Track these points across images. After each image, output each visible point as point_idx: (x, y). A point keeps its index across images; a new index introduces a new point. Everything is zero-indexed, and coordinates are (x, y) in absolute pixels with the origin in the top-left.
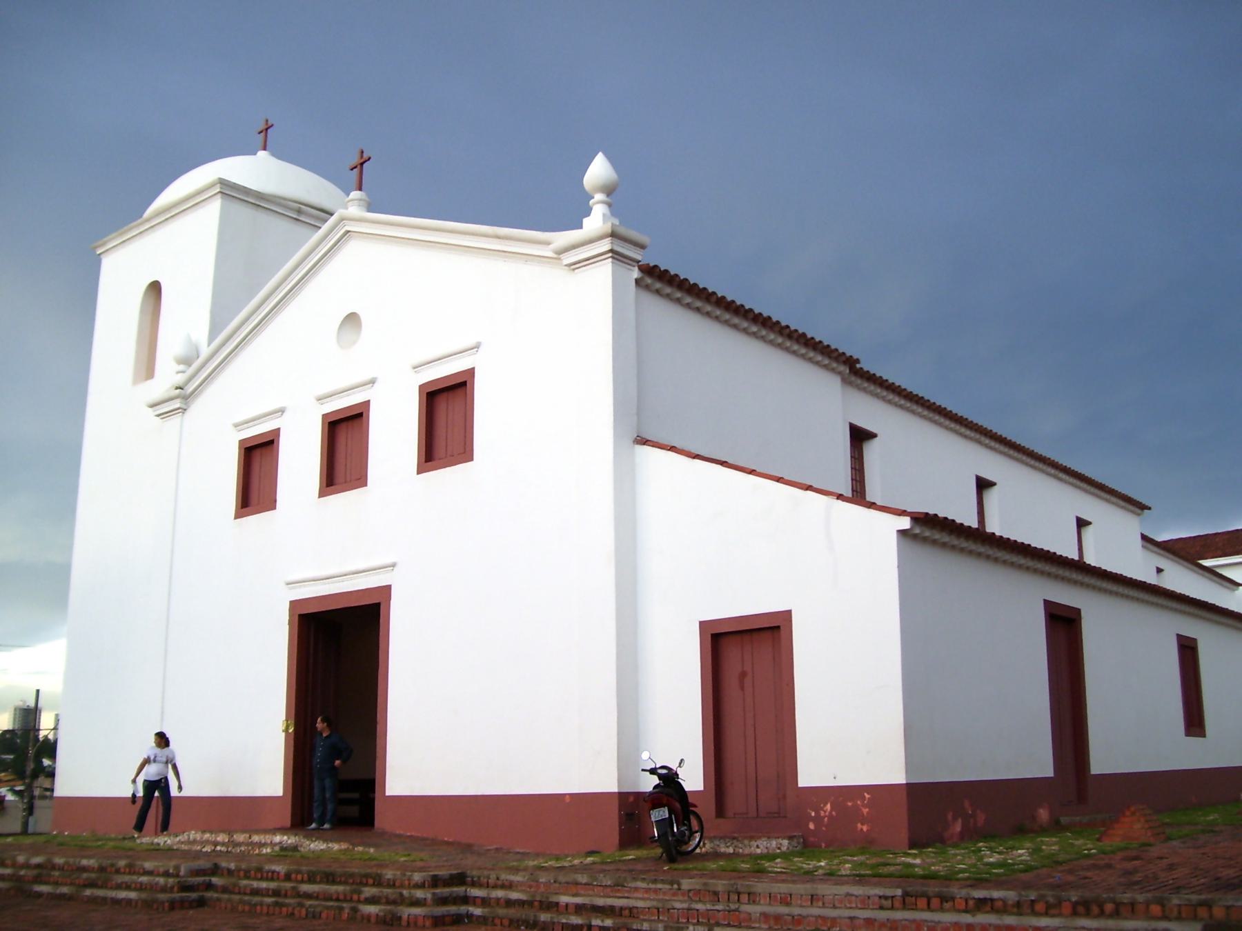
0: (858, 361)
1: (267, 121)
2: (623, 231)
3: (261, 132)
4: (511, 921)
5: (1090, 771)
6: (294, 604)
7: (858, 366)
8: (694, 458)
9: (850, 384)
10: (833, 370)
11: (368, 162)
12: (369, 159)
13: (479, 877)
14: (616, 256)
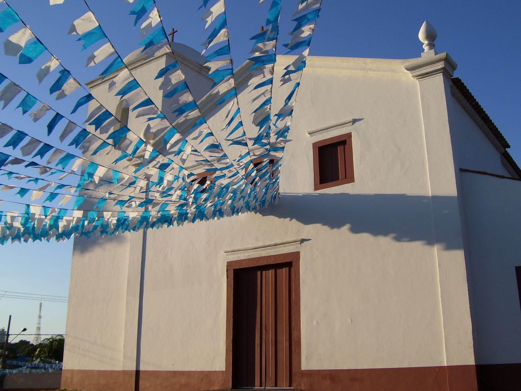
1: (173, 29)
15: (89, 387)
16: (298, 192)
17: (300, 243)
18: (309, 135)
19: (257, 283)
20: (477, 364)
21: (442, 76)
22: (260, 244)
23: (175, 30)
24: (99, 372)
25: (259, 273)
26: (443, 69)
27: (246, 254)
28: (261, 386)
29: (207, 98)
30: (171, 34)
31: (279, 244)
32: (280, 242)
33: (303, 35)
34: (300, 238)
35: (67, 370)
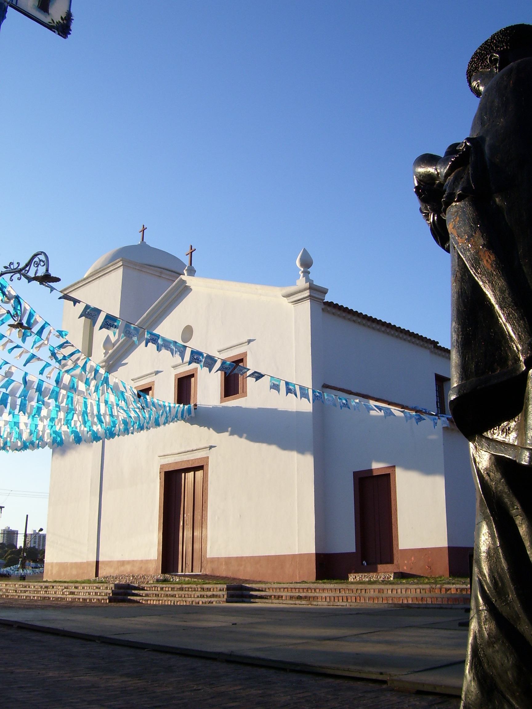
0: (438, 343)
1: (144, 226)
2: (312, 294)
4: (156, 594)
5: (398, 545)
7: (438, 345)
8: (350, 394)
10: (425, 347)
11: (194, 252)
12: (195, 250)
13: (142, 594)
14: (312, 298)
17: (209, 449)
18: (218, 353)
20: (320, 552)
21: (310, 302)
23: (145, 227)
24: (72, 564)
25: (183, 474)
26: (310, 296)
27: (173, 459)
28: (182, 572)
29: (147, 315)
30: (141, 231)
31: (195, 450)
32: (195, 449)
33: (482, 90)
34: (208, 445)
35: (48, 563)
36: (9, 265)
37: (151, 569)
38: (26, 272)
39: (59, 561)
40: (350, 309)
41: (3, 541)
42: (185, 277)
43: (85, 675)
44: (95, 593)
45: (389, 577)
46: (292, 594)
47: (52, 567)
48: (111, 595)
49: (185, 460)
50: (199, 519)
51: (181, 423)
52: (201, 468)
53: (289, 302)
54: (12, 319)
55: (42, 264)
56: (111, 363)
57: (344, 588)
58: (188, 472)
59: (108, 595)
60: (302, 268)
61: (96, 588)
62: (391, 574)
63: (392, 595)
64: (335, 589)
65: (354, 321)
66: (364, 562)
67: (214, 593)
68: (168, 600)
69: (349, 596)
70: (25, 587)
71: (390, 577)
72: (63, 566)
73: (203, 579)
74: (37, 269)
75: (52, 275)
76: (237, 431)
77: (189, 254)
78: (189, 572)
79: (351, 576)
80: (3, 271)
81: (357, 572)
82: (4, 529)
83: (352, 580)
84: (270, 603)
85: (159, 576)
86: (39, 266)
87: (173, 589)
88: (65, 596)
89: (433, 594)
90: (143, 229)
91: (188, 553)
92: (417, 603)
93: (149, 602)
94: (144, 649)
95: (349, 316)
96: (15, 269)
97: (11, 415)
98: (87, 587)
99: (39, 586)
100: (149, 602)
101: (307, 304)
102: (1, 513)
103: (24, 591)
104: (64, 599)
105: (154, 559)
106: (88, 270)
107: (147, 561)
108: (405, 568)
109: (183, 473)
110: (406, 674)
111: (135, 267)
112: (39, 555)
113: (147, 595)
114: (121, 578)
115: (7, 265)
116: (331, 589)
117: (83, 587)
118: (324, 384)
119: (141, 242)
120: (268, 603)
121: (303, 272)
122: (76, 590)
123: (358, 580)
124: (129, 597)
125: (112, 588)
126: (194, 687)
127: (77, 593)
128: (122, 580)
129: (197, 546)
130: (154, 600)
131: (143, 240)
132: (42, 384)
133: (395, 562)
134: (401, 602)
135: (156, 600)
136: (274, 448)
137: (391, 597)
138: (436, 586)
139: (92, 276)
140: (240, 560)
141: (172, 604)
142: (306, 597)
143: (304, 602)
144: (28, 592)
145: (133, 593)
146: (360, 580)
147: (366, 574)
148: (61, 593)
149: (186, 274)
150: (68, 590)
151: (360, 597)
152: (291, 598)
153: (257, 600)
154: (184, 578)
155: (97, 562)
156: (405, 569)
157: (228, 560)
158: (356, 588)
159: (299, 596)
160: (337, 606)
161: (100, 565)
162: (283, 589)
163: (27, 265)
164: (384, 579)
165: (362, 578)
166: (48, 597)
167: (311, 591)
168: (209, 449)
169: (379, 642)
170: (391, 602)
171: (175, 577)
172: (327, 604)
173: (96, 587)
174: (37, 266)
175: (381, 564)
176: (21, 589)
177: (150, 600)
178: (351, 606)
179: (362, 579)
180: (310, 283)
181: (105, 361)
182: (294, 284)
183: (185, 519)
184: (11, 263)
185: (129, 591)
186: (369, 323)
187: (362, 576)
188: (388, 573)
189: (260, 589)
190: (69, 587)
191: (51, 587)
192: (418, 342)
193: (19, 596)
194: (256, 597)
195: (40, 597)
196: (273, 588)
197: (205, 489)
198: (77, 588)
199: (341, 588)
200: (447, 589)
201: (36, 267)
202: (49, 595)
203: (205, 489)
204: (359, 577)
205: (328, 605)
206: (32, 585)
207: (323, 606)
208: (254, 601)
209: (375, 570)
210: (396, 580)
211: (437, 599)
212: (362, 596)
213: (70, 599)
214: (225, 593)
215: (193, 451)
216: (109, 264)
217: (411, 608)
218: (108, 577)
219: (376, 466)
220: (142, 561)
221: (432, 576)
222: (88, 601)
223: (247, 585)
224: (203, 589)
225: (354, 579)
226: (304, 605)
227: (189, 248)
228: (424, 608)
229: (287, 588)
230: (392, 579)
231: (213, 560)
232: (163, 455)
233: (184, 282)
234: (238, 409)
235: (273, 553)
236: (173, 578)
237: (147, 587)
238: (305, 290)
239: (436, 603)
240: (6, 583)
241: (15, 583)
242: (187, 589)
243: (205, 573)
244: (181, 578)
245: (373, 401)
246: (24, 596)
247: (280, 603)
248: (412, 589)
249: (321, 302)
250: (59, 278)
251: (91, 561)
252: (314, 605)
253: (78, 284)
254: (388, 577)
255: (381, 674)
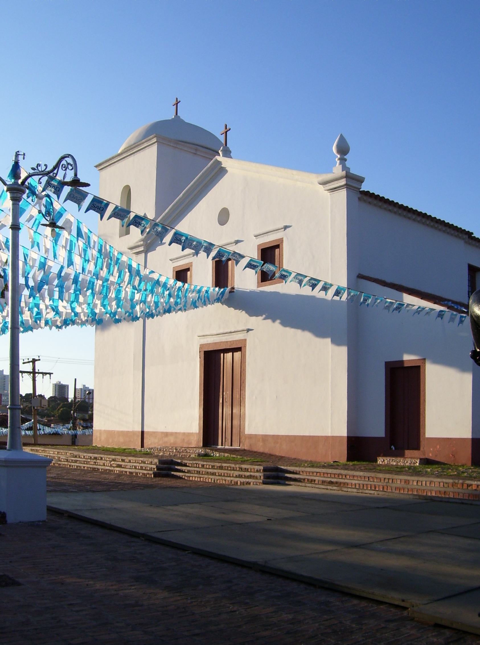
0: (472, 233)
1: (177, 99)
3: (175, 105)
4: (197, 471)
5: (424, 433)
6: (202, 346)
9: (469, 244)
10: (460, 238)
11: (229, 131)
12: (230, 129)
13: (185, 470)
14: (348, 187)
15: (112, 444)
16: (247, 288)
17: (247, 332)
18: (255, 238)
19: (221, 363)
21: (346, 191)
22: (221, 331)
23: (178, 100)
25: (222, 354)
26: (346, 185)
27: (212, 339)
28: (222, 445)
29: (183, 195)
31: (233, 332)
32: (233, 331)
35: (97, 430)
36: (36, 166)
37: (193, 441)
38: (55, 175)
39: (107, 429)
40: (386, 198)
41: (55, 394)
42: (220, 158)
43: (130, 588)
44: (141, 467)
45: (415, 462)
46: (324, 479)
47: (100, 434)
48: (156, 470)
49: (223, 341)
50: (238, 397)
51: (218, 305)
52: (239, 349)
53: (325, 189)
54: (44, 219)
55: (70, 167)
56: (149, 242)
57: (372, 476)
58: (226, 353)
59: (153, 470)
60: (339, 154)
61: (142, 462)
62: (417, 460)
63: (417, 487)
64: (365, 477)
65: (390, 210)
66: (392, 447)
67: (252, 474)
68: (209, 478)
69: (377, 485)
70: (76, 457)
71: (416, 462)
72: (111, 434)
73: (241, 456)
74: (66, 173)
75: (81, 181)
76: (272, 316)
77: (223, 133)
78: (228, 446)
79: (380, 459)
80: (31, 172)
81: (385, 455)
82: (55, 383)
83: (381, 463)
84: (303, 486)
85: (201, 451)
86: (67, 169)
87: (213, 467)
88: (112, 468)
89: (456, 490)
90: (177, 102)
91: (227, 429)
92: (440, 496)
93: (191, 478)
94: (184, 550)
95: (385, 206)
96: (43, 171)
97: (51, 301)
98: (133, 460)
99: (89, 457)
100: (191, 478)
101: (343, 194)
102: (50, 379)
103: (75, 460)
104: (112, 472)
105: (195, 432)
106: (121, 146)
107: (189, 434)
108: (431, 455)
109: (222, 353)
110: (426, 604)
111: (169, 144)
112: (90, 408)
113: (189, 472)
114: (165, 450)
115: (35, 166)
116: (361, 476)
117: (129, 461)
118: (359, 274)
119: (175, 116)
120: (302, 486)
121: (340, 159)
122: (123, 463)
123: (386, 463)
124: (172, 473)
125: (156, 463)
126: (230, 607)
127: (124, 465)
128: (166, 452)
129: (236, 422)
130: (195, 477)
131: (177, 114)
132: (78, 276)
133: (421, 449)
134: (425, 494)
135: (198, 477)
136: (308, 335)
137: (416, 489)
138: (458, 481)
139: (126, 152)
140: (276, 438)
141: (213, 481)
142: (337, 483)
143: (335, 488)
144: (79, 462)
145: (176, 468)
146: (388, 463)
147: (394, 458)
148: (109, 465)
149: (221, 155)
150: (116, 463)
151: (387, 487)
152: (323, 482)
153: (291, 483)
154: (224, 454)
155: (143, 432)
156: (430, 456)
157: (265, 438)
158: (384, 477)
159: (330, 481)
160: (366, 493)
161: (145, 435)
162: (316, 473)
163: (54, 168)
164: (410, 463)
165: (390, 461)
166: (97, 468)
167: (342, 476)
168: (247, 332)
169: (402, 553)
170: (415, 493)
171: (215, 452)
172: (356, 491)
173: (141, 461)
174: (66, 170)
175: (408, 450)
176: (72, 459)
177: (192, 477)
178: (378, 494)
179: (390, 463)
180: (346, 172)
181: (143, 240)
182: (331, 172)
183: (224, 396)
184: (38, 164)
185: (172, 466)
186: (405, 213)
187: (390, 460)
188: (415, 459)
189: (295, 471)
190: (116, 459)
191: (100, 459)
192: (453, 232)
193: (70, 466)
194: (291, 479)
195: (90, 468)
196: (306, 472)
197: (243, 370)
198: (124, 461)
199: (370, 476)
200: (469, 485)
201: (64, 170)
202: (98, 467)
203: (243, 370)
204: (387, 461)
205: (357, 492)
206: (82, 455)
207: (353, 493)
208: (289, 484)
209: (402, 455)
210: (421, 466)
211: (459, 494)
212: (389, 486)
213: (118, 472)
214: (261, 474)
215: (231, 333)
216: (143, 139)
217: (434, 501)
218: (152, 448)
219: (408, 357)
220: (184, 434)
221: (456, 464)
222: (134, 474)
223: (283, 467)
224: (241, 469)
225: (382, 462)
226: (335, 490)
227: (224, 128)
228: (445, 502)
229: (320, 472)
230: (418, 464)
231: (251, 437)
232: (202, 335)
233: (219, 163)
234: (276, 294)
235: (307, 434)
236: (213, 453)
237: (189, 464)
238: (341, 178)
239: (457, 497)
240: (58, 451)
241: (67, 451)
242: (226, 468)
243: (243, 448)
244: (221, 453)
245: (407, 295)
246: (74, 466)
247: (313, 487)
248: (436, 482)
249: (357, 191)
250: (89, 183)
251: (136, 431)
252: (345, 491)
253: (113, 160)
254: (414, 462)
255: (403, 601)
